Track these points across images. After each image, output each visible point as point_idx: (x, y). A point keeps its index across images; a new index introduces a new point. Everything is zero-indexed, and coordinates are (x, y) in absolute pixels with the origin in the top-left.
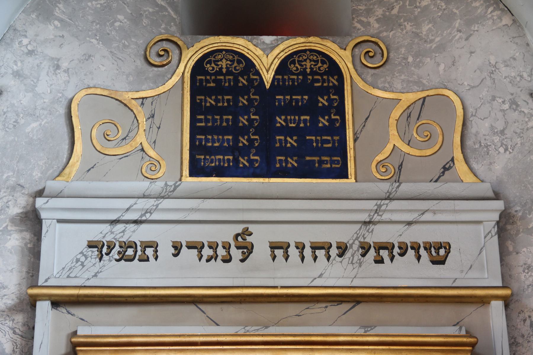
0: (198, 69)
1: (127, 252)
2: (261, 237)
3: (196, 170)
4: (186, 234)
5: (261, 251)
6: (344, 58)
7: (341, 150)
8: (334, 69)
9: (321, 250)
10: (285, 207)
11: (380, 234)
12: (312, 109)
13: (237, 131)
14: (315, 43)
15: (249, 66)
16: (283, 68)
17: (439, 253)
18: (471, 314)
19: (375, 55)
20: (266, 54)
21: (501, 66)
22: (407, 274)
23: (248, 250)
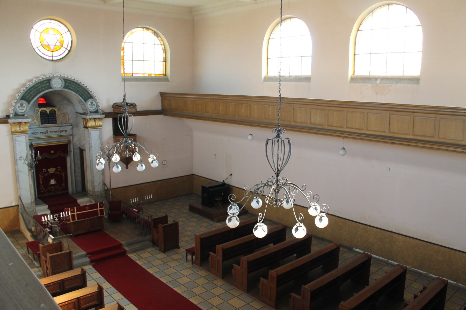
0: (41, 112)
1: (35, 133)
2: (49, 131)
3: (42, 124)
4: (41, 131)
5: (49, 132)
6: (56, 110)
7: (56, 120)
8: (55, 111)
9: (312, 243)
10: (52, 129)
11: (60, 130)
12: (53, 116)
13: (45, 119)
14: (53, 108)
15: (46, 112)
16: (50, 112)
17: (66, 131)
18: (69, 137)
19: (59, 109)
20: (48, 110)
21: (187, 240)
22: (63, 133)
23: (47, 132)
